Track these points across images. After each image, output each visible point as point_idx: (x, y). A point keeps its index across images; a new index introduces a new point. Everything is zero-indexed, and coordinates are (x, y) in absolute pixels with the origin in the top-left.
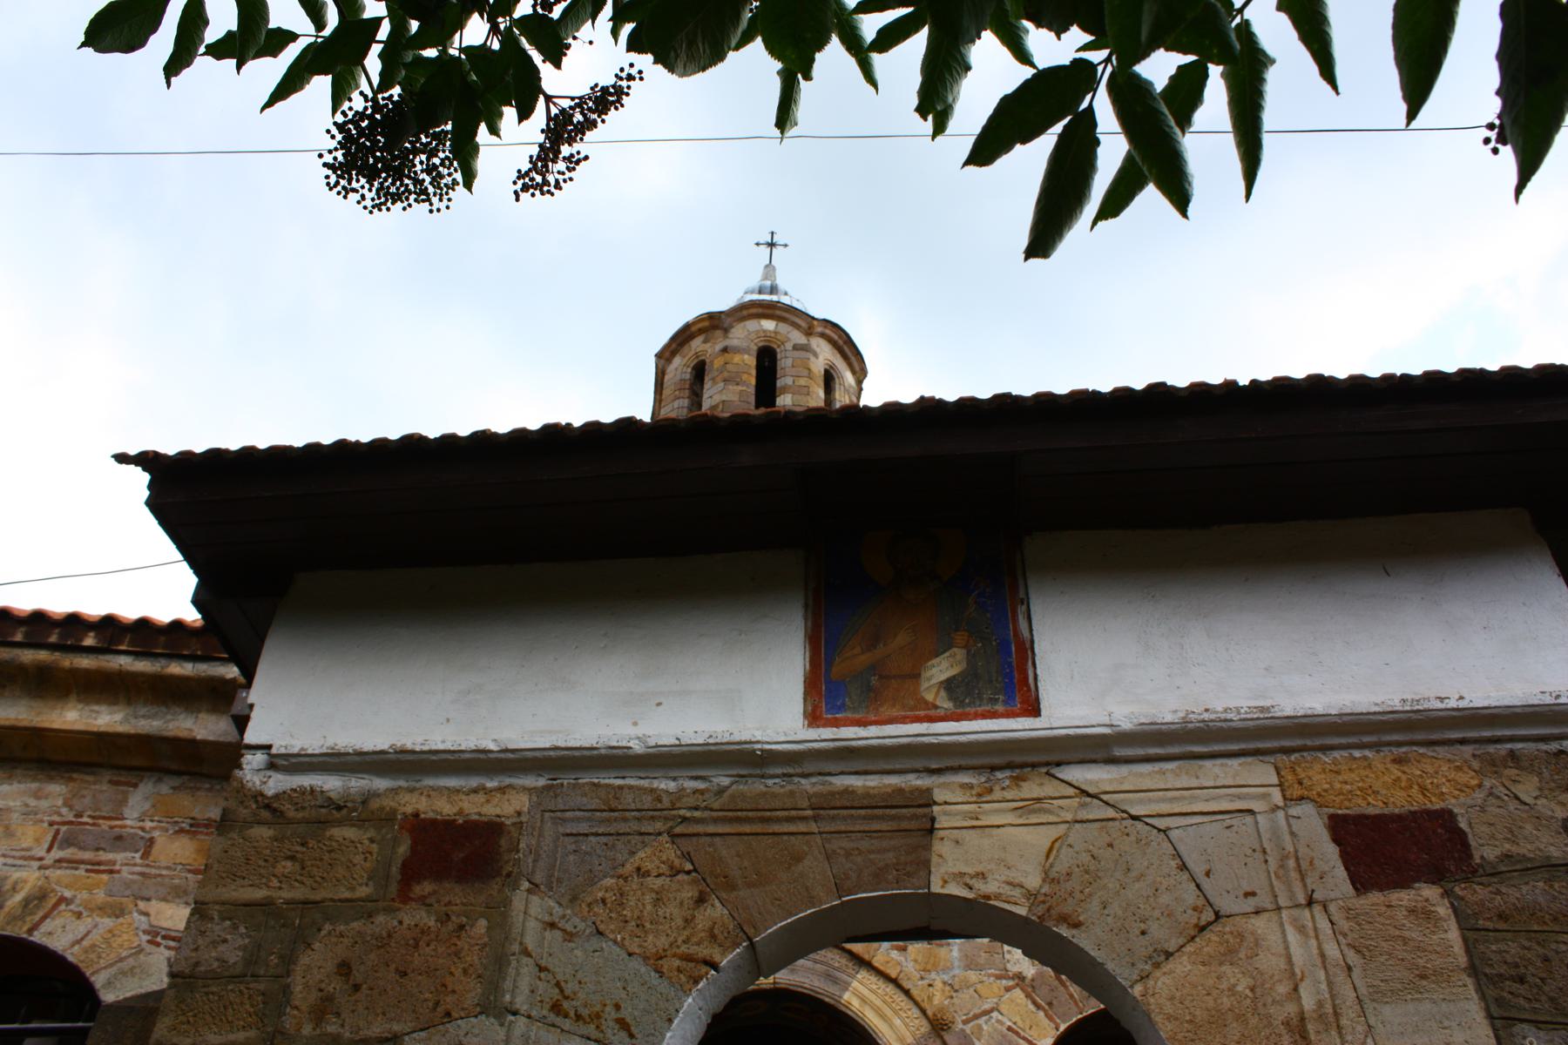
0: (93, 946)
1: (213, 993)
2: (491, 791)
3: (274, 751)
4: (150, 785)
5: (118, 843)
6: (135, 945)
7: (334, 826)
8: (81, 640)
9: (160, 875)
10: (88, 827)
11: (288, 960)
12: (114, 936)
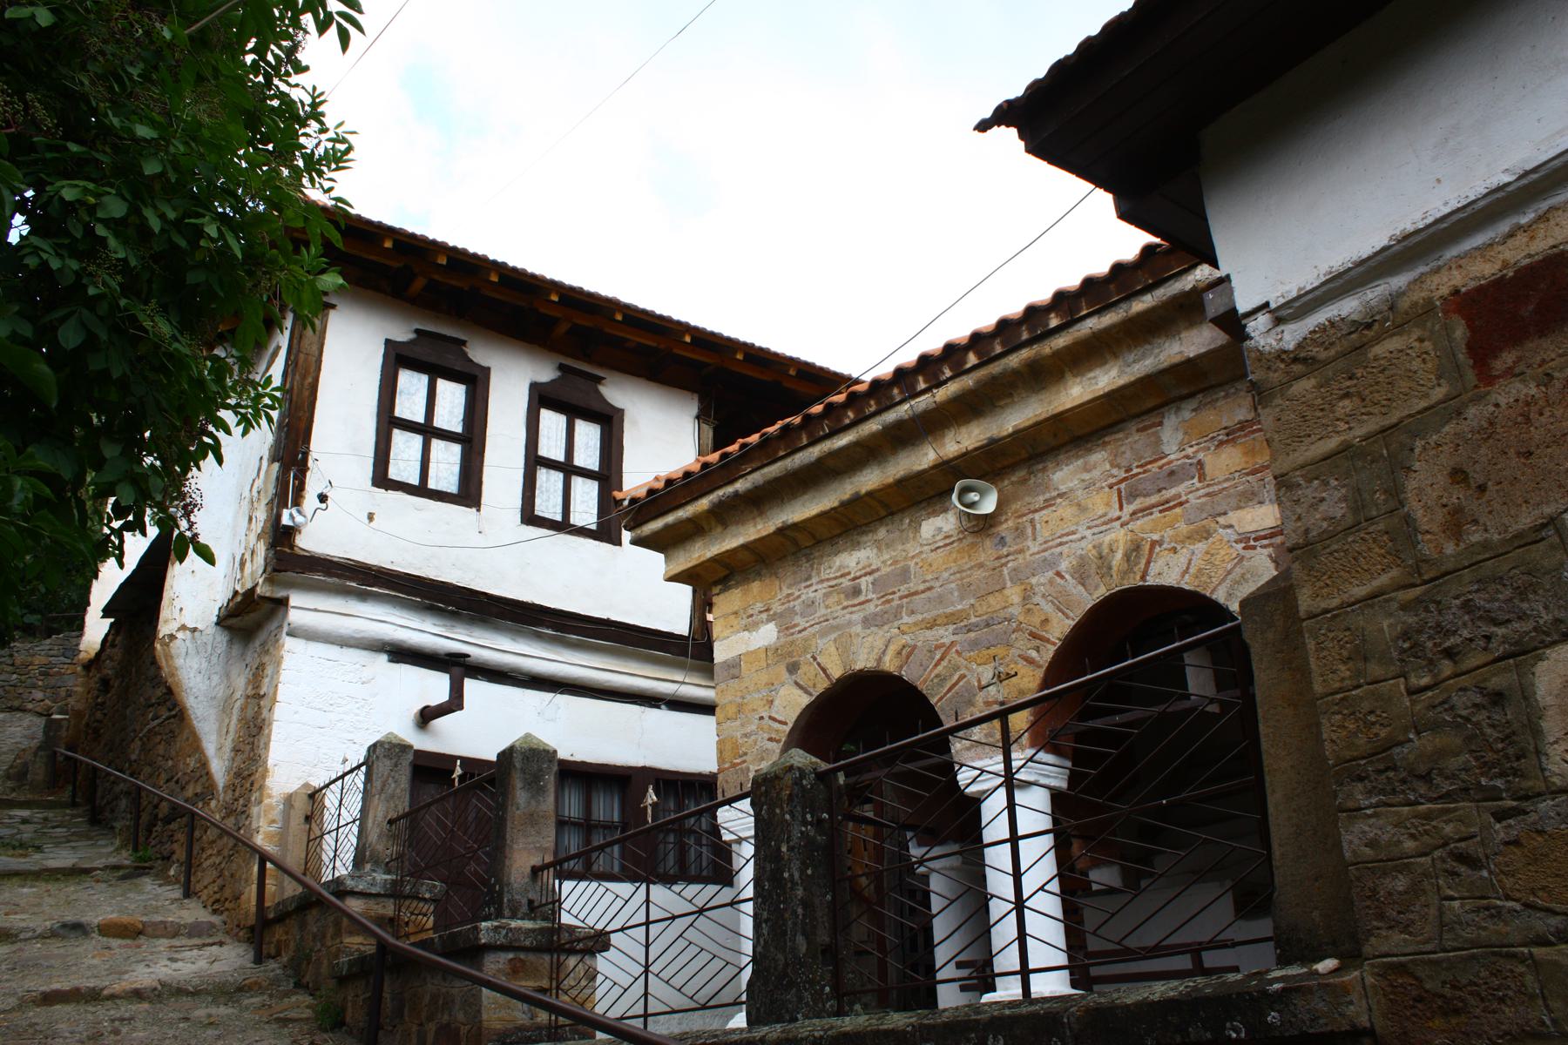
0: (1200, 570)
1: (1335, 551)
2: (1530, 226)
3: (1273, 306)
4: (1173, 417)
5: (1173, 478)
6: (1234, 555)
7: (1373, 346)
8: (1048, 325)
9: (1224, 489)
10: (1141, 476)
11: (1395, 493)
12: (1212, 555)
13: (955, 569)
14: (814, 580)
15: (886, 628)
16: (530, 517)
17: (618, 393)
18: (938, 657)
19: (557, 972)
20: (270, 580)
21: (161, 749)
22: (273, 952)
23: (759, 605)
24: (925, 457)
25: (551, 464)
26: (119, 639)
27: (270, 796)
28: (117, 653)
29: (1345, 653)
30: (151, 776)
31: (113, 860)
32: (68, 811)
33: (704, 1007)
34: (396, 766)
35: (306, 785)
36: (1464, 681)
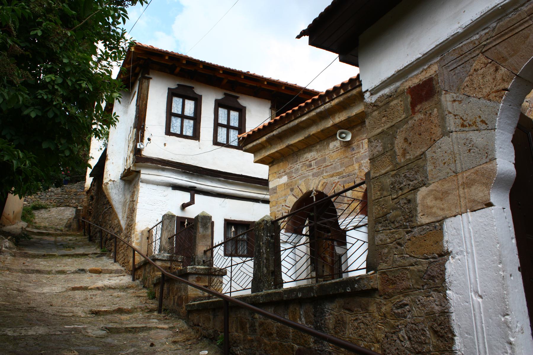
11: (392, 144)
13: (339, 158)
14: (298, 162)
15: (319, 177)
16: (216, 143)
17: (244, 101)
18: (334, 186)
19: (210, 282)
20: (134, 165)
21: (108, 218)
22: (138, 277)
23: (282, 170)
24: (329, 123)
25: (223, 126)
26: (95, 183)
27: (137, 231)
28: (95, 188)
29: (379, 189)
30: (105, 226)
31: (95, 252)
32: (83, 237)
33: (244, 289)
34: (171, 221)
35: (147, 228)
36: (403, 197)
